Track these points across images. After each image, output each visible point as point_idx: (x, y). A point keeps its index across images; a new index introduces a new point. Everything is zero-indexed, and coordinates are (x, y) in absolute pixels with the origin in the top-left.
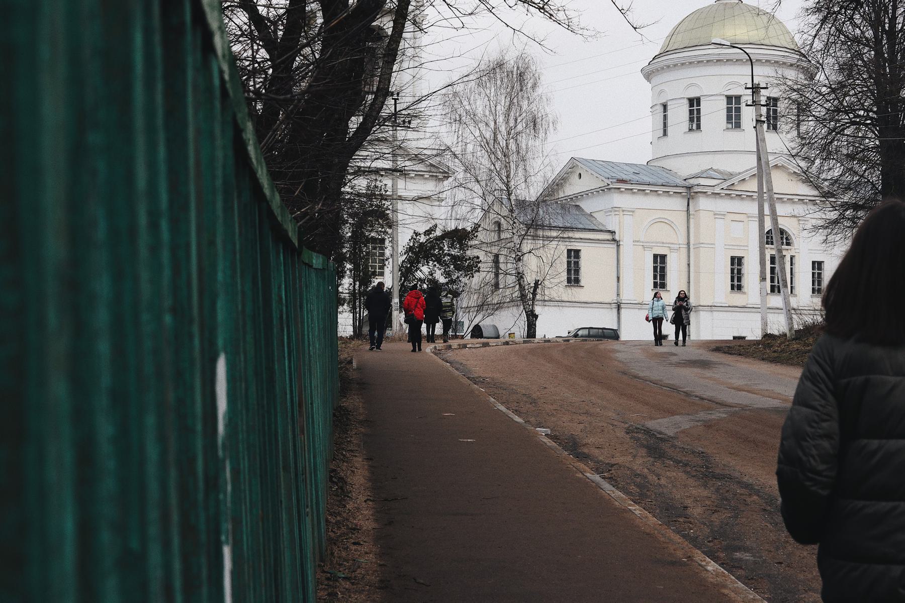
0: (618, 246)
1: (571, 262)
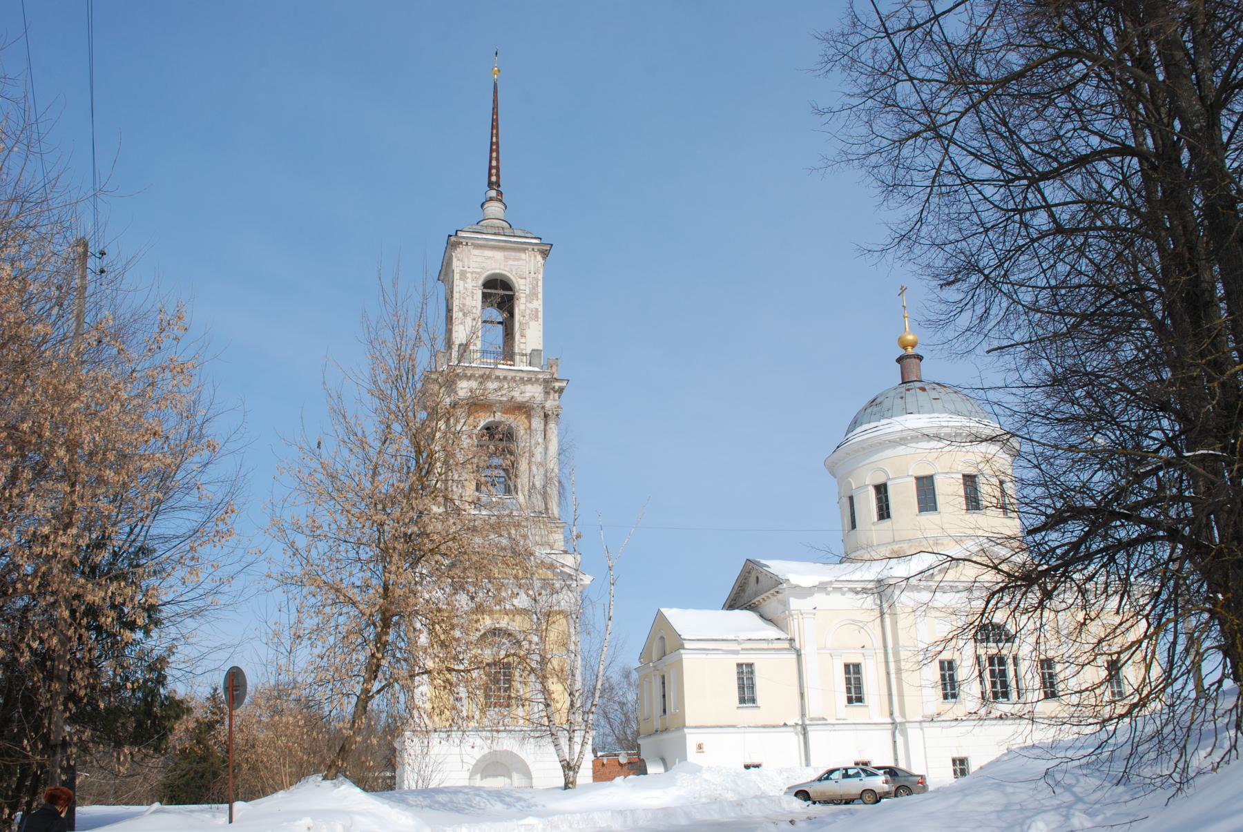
0: (799, 655)
1: (854, 673)
